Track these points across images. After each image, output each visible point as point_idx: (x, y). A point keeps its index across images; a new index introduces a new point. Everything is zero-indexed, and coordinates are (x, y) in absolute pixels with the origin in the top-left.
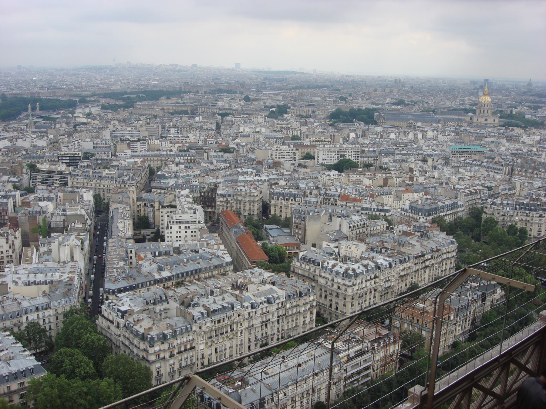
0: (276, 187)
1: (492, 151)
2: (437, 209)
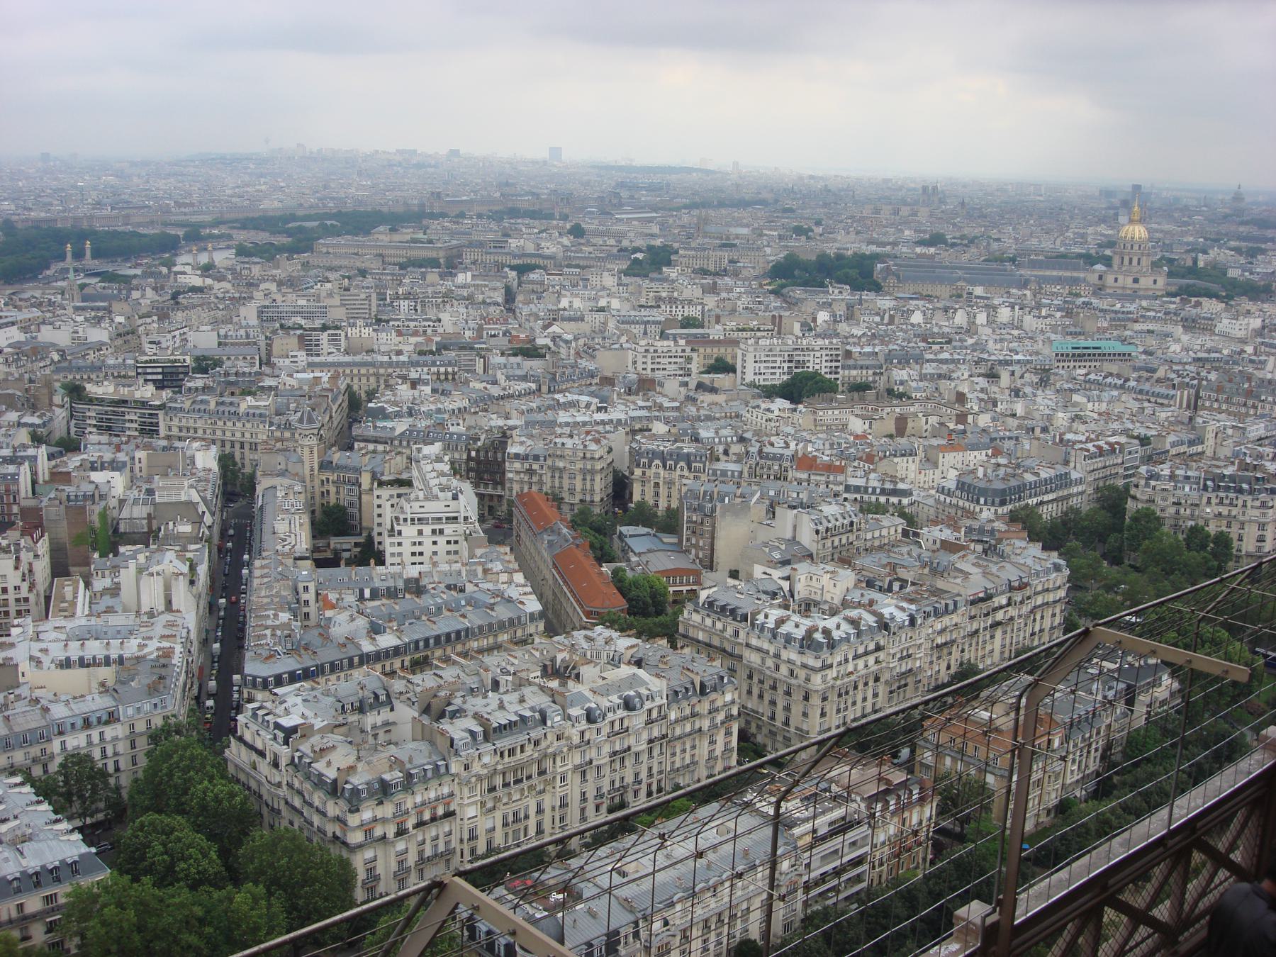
0: (644, 437)
1: (1150, 353)
2: (1021, 490)
